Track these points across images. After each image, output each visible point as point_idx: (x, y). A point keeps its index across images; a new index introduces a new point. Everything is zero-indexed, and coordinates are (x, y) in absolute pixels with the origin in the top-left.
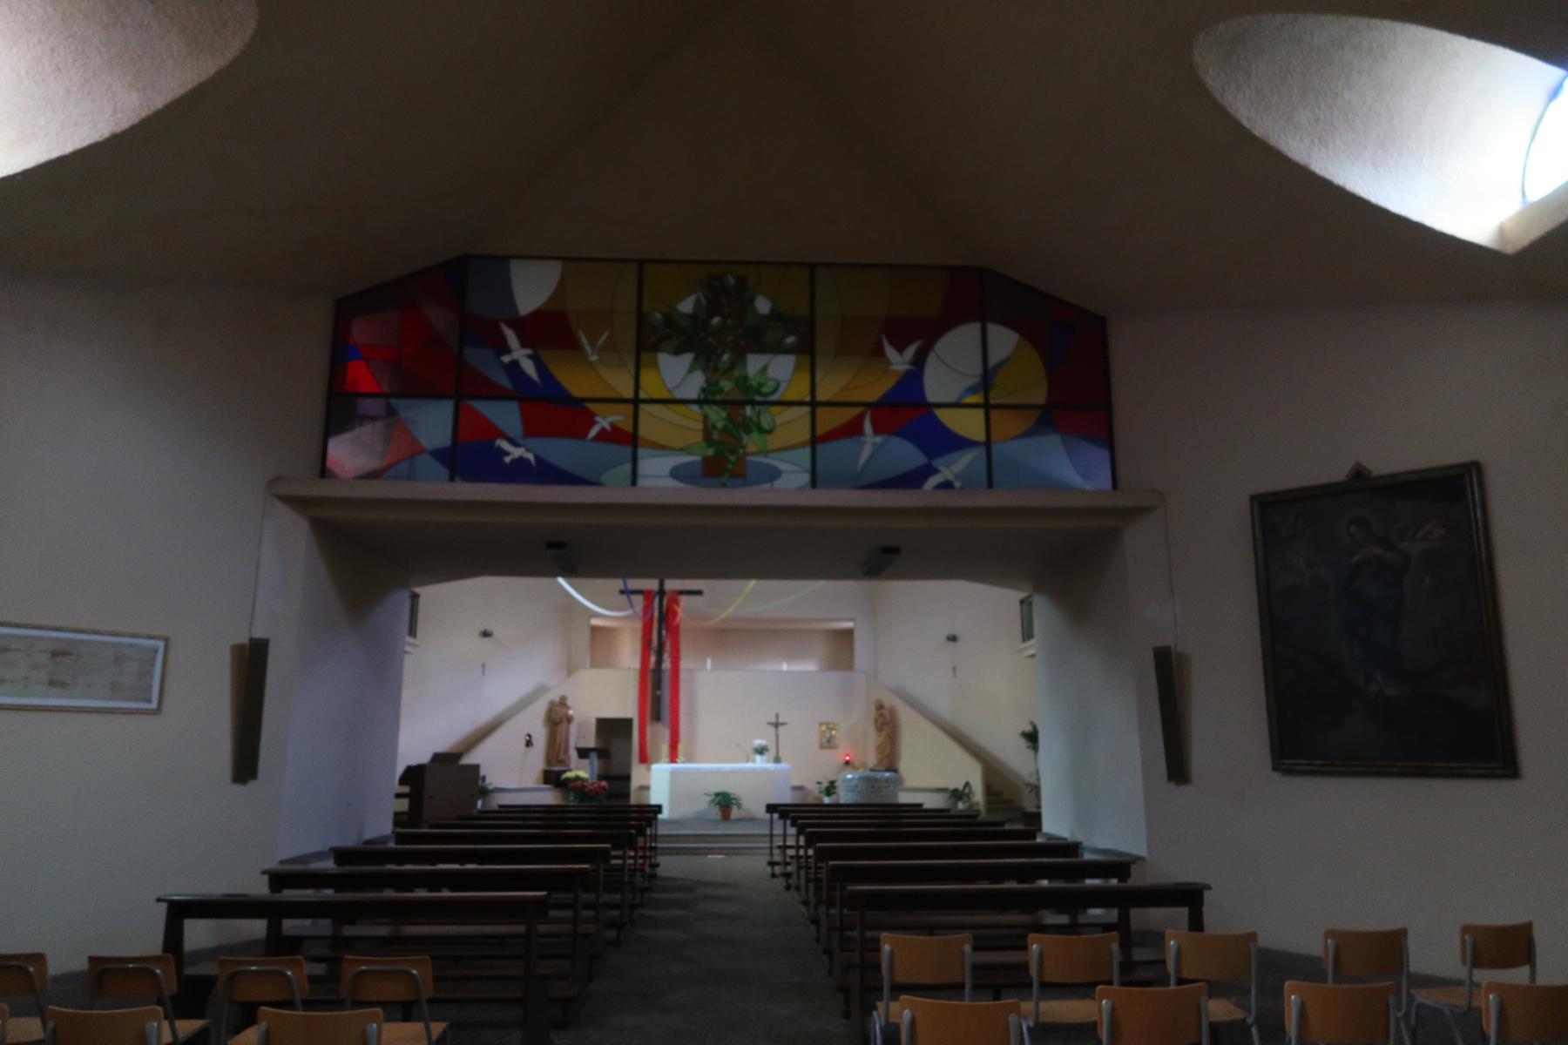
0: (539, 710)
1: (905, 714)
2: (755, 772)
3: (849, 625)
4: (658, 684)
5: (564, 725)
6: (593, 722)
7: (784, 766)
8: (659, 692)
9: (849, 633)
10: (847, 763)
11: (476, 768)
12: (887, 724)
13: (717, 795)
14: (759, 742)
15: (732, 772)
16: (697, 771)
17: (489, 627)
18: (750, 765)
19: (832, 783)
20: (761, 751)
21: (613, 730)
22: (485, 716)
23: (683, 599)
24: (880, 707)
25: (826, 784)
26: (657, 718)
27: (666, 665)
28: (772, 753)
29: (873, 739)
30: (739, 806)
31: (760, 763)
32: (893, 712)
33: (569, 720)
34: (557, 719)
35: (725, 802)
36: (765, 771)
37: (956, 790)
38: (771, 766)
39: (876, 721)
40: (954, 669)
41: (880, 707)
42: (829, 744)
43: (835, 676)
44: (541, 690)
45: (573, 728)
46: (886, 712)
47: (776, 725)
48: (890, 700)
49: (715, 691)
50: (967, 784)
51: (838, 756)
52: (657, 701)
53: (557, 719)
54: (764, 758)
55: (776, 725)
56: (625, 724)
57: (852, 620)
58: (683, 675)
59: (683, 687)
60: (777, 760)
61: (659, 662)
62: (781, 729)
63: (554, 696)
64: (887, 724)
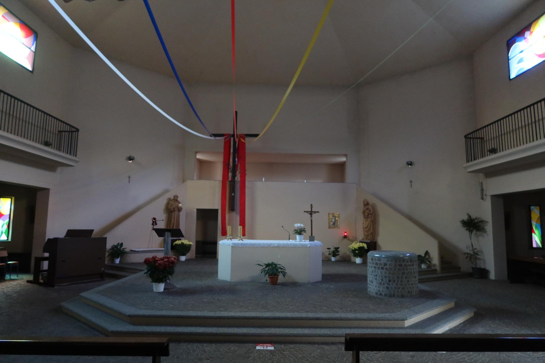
0: (162, 203)
1: (382, 209)
2: (295, 247)
3: (344, 159)
4: (233, 189)
5: (176, 213)
6: (195, 210)
7: (316, 242)
8: (234, 195)
9: (342, 166)
10: (345, 237)
11: (106, 238)
12: (370, 214)
13: (268, 265)
14: (298, 225)
15: (278, 247)
16: (253, 246)
17: (133, 155)
18: (291, 242)
19: (337, 249)
20: (300, 232)
21: (206, 216)
22: (131, 207)
23: (247, 139)
24: (366, 204)
25: (332, 249)
26: (232, 209)
27: (238, 178)
28: (308, 233)
29: (361, 223)
30: (284, 274)
31: (298, 241)
32: (374, 207)
33: (180, 210)
34: (172, 209)
35: (273, 271)
36: (304, 247)
37: (419, 256)
38: (307, 242)
39: (364, 212)
40: (411, 182)
41: (366, 204)
42: (334, 225)
43: (336, 186)
44: (167, 191)
45: (182, 214)
46: (370, 207)
47: (311, 213)
48: (372, 200)
49: (265, 194)
50: (427, 253)
51: (340, 232)
52: (232, 199)
53: (172, 209)
54: (302, 237)
55: (311, 213)
56: (214, 212)
57: (346, 155)
58: (247, 184)
59: (247, 191)
60: (312, 239)
61: (234, 176)
62: (314, 215)
63: (170, 195)
64: (370, 214)
